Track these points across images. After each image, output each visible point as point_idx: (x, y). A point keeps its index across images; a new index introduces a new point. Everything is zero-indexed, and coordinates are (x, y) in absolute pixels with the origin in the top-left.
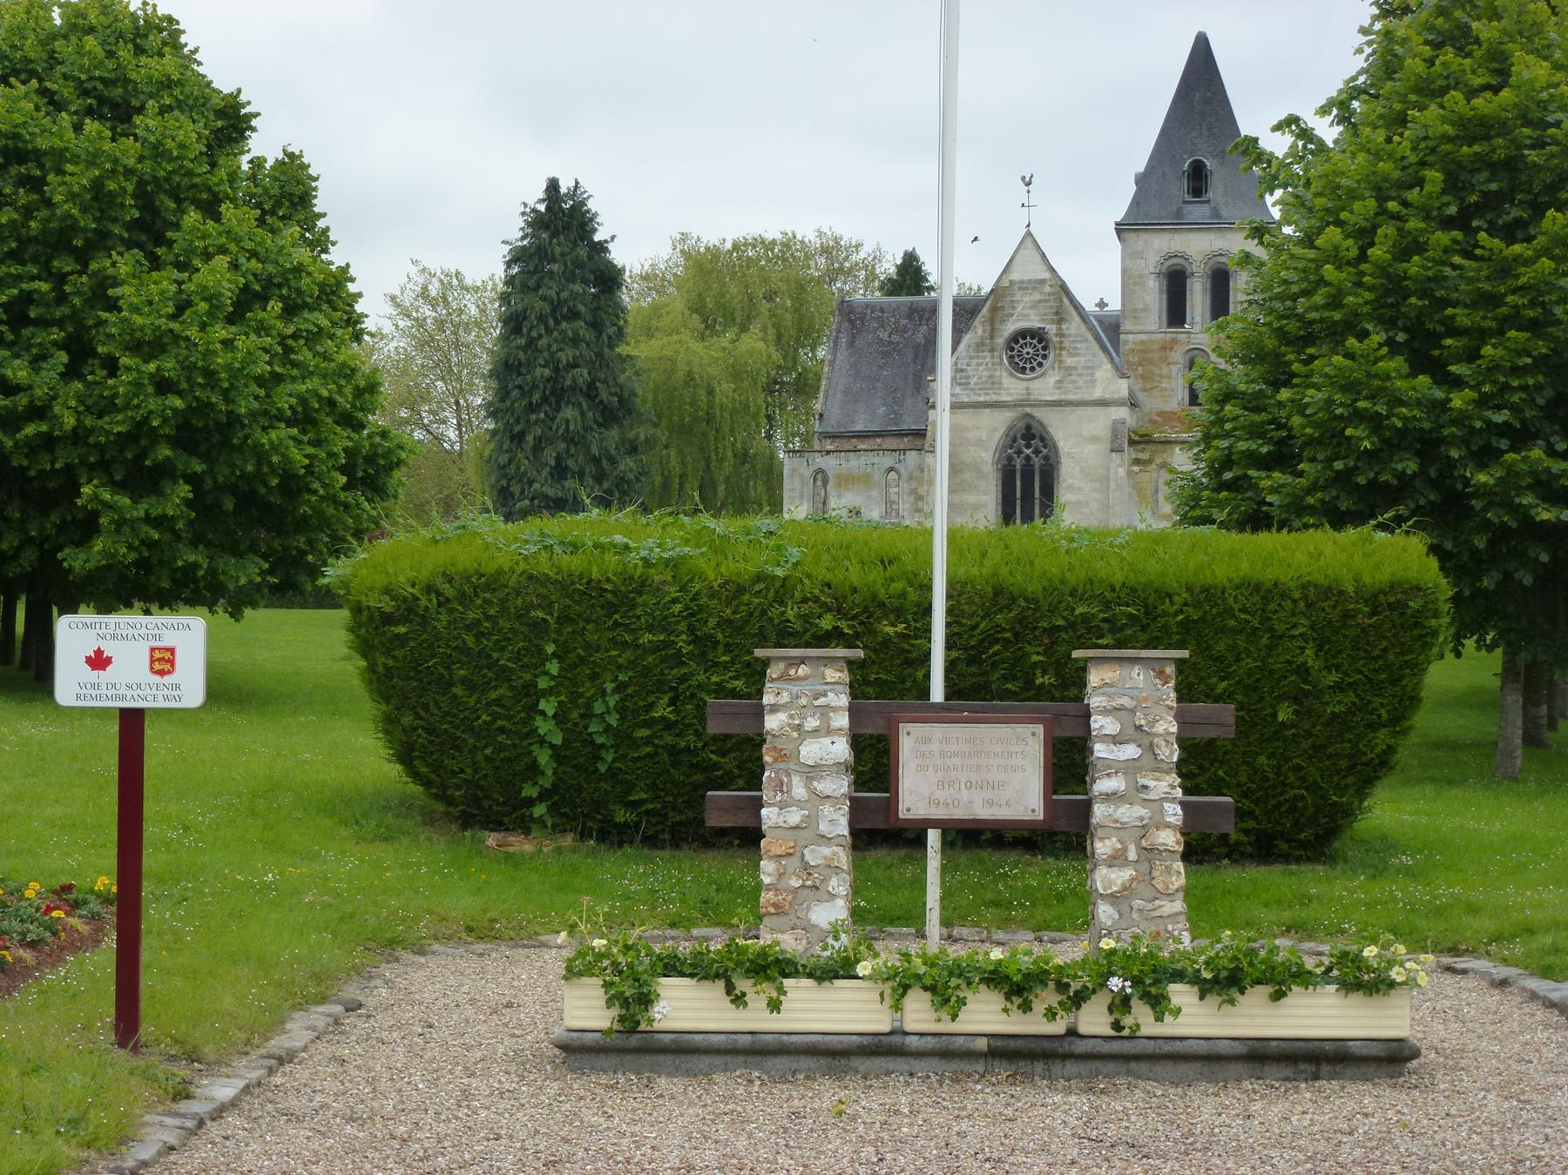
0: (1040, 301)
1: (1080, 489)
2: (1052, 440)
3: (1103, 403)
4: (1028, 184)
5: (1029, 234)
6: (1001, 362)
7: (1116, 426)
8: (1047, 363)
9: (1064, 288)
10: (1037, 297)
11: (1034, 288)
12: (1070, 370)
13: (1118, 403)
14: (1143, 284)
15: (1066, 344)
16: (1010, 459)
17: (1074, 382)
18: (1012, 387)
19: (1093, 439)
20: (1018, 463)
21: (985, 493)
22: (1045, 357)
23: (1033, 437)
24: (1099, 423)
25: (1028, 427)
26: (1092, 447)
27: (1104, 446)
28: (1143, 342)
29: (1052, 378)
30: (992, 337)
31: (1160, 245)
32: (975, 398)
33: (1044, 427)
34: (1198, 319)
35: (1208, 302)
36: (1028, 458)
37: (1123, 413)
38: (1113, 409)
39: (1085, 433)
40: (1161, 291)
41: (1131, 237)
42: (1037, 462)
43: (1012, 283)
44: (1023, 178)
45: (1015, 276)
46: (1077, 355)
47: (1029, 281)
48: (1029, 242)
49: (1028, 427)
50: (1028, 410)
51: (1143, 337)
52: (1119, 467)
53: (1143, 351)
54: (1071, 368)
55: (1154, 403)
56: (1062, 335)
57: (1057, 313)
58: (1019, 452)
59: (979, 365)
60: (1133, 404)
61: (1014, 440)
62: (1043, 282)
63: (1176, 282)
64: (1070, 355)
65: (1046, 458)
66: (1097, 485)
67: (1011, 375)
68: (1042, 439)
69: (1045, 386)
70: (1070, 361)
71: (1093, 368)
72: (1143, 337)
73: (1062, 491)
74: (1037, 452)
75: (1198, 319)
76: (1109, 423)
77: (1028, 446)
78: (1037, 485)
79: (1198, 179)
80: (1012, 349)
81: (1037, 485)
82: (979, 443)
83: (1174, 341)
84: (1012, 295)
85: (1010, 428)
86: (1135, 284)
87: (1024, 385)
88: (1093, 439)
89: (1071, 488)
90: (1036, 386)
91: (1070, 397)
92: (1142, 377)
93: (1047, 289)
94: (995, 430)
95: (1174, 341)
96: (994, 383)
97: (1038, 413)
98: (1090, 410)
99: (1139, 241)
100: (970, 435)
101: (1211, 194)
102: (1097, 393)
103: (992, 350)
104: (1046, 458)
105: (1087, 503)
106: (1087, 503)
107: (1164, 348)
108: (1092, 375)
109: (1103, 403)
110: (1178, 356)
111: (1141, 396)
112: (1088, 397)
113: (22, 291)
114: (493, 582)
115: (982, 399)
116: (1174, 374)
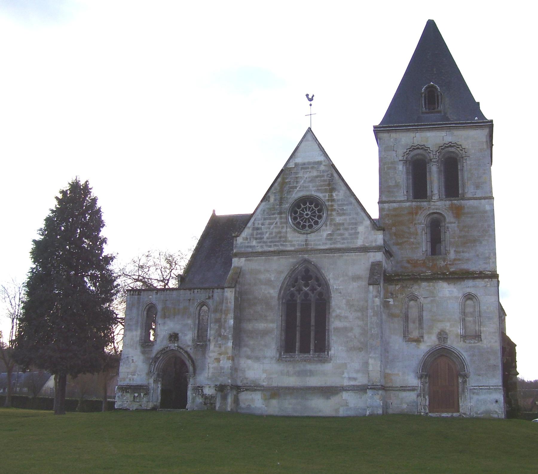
0: (317, 177)
1: (346, 317)
2: (325, 279)
3: (364, 249)
4: (311, 100)
5: (310, 130)
6: (287, 222)
7: (375, 267)
8: (321, 222)
9: (333, 166)
10: (315, 173)
11: (312, 168)
12: (338, 226)
13: (378, 249)
14: (395, 169)
15: (336, 207)
16: (292, 295)
17: (341, 235)
18: (295, 239)
19: (356, 278)
20: (299, 299)
21: (272, 321)
22: (320, 217)
23: (310, 278)
24: (361, 264)
25: (307, 271)
26: (355, 284)
27: (364, 283)
28: (395, 209)
29: (325, 232)
30: (281, 204)
31: (407, 139)
32: (266, 249)
33: (318, 269)
34: (436, 191)
35: (443, 180)
36: (306, 294)
37: (379, 256)
38: (372, 254)
39: (350, 274)
40: (407, 173)
41: (385, 135)
42: (313, 297)
43: (296, 165)
44: (307, 95)
45: (299, 160)
46: (344, 214)
47: (309, 163)
48: (309, 137)
49: (307, 271)
50: (306, 256)
51: (395, 205)
52: (374, 297)
53: (396, 216)
54: (340, 224)
55: (403, 254)
56: (333, 200)
57: (329, 185)
58: (299, 290)
59: (271, 224)
60: (388, 254)
61: (296, 280)
62: (319, 163)
63: (418, 167)
64: (339, 215)
65: (320, 294)
66: (359, 314)
67: (295, 230)
68: (317, 279)
69: (320, 238)
70: (338, 219)
71: (356, 224)
72: (395, 205)
73: (332, 320)
74: (313, 290)
75: (436, 191)
76: (368, 265)
77: (306, 285)
78: (313, 315)
79: (432, 99)
80: (296, 212)
81: (313, 315)
82: (269, 283)
83: (419, 208)
84: (296, 173)
85: (293, 271)
86: (389, 168)
87: (302, 237)
88: (356, 278)
89: (338, 317)
90: (312, 237)
91: (339, 246)
92: (395, 234)
93: (322, 168)
94: (282, 272)
95: (419, 208)
96: (281, 238)
97: (314, 258)
98: (353, 256)
99: (391, 138)
100: (262, 277)
101: (441, 108)
102: (360, 243)
103: (280, 213)
104: (320, 294)
105: (352, 329)
106: (352, 329)
107: (411, 213)
108: (356, 228)
109: (364, 249)
110: (422, 220)
111: (395, 249)
112: (352, 246)
113: (114, 320)
114: (350, 417)
115: (272, 249)
116: (419, 231)
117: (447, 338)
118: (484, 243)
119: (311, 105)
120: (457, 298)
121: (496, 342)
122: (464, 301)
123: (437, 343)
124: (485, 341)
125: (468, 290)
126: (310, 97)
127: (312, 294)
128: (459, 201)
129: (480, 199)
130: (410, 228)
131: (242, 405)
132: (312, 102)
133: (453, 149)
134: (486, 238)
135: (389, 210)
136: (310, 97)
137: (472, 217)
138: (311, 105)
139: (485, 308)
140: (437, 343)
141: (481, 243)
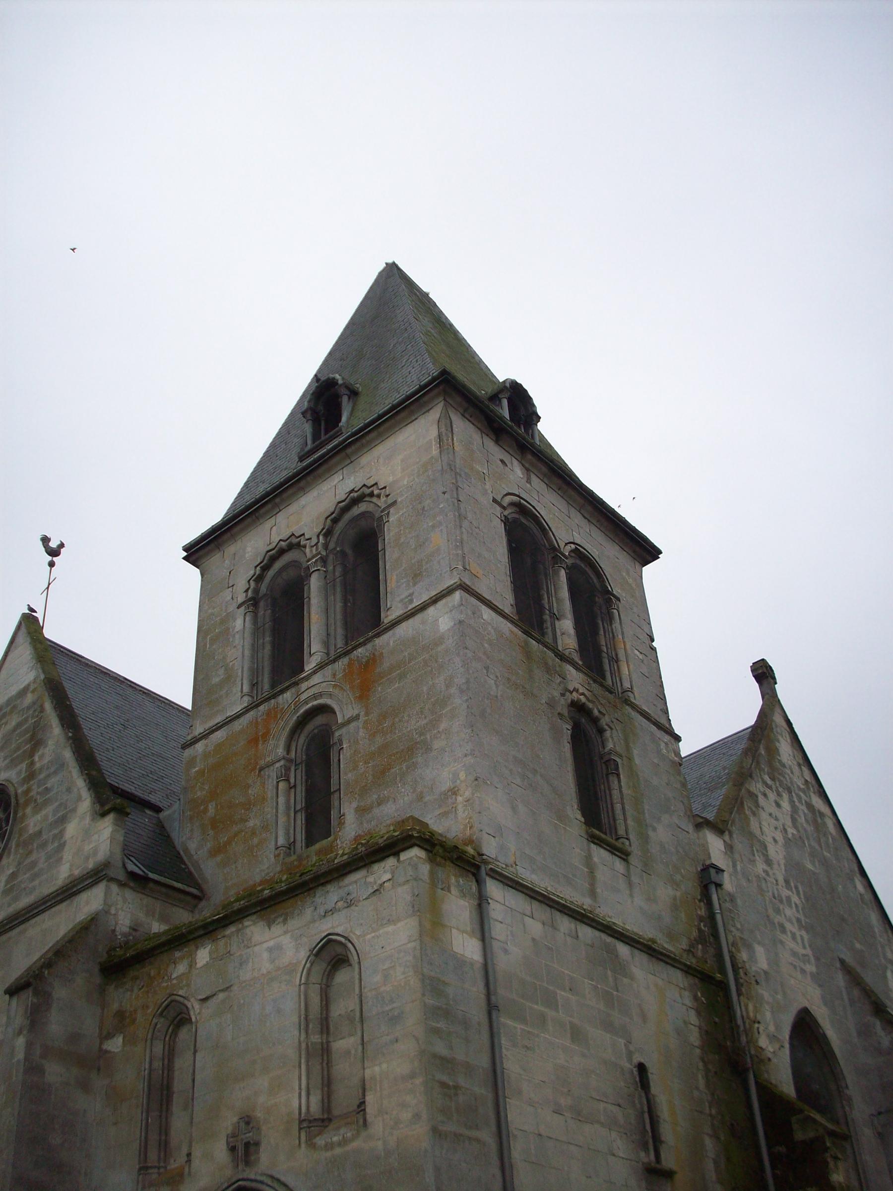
4: (54, 553)
44: (45, 540)
57: (32, 737)
107: (254, 741)
117: (257, 1144)
118: (437, 744)
119: (52, 564)
120: (290, 970)
121: (417, 1116)
122: (316, 977)
123: (228, 1172)
124: (377, 1126)
125: (326, 927)
126: (53, 544)
127: (551, 1028)
128: (369, 646)
129: (423, 608)
130: (248, 786)
131: (664, 1162)
132: (55, 559)
133: (362, 507)
134: (443, 726)
135: (206, 755)
136: (53, 544)
137: (402, 677)
138: (52, 564)
139: (378, 978)
140: (228, 1172)
141: (428, 749)
